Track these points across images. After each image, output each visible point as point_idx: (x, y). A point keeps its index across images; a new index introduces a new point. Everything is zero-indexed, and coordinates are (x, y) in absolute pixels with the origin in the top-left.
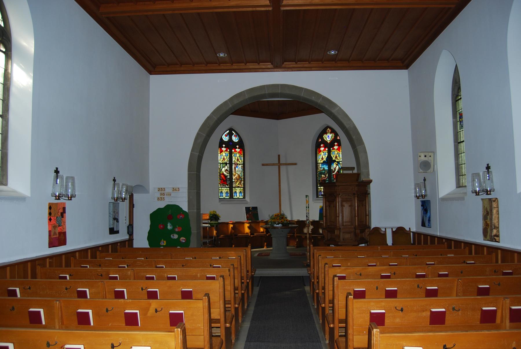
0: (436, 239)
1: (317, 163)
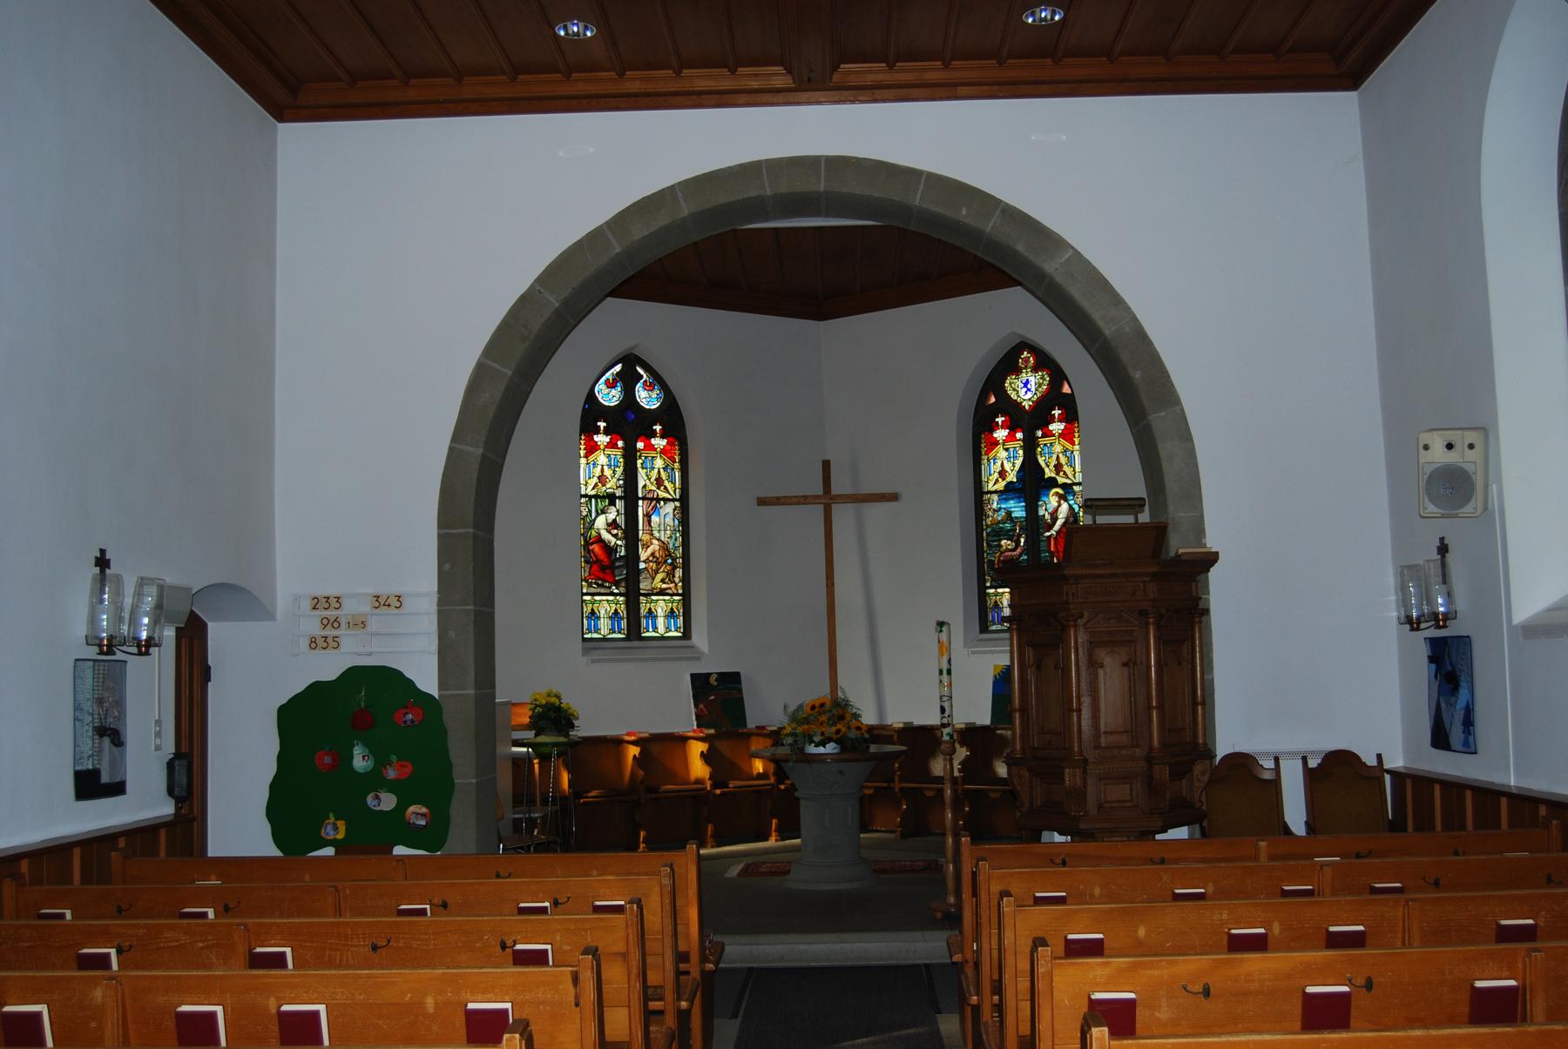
1: (979, 492)
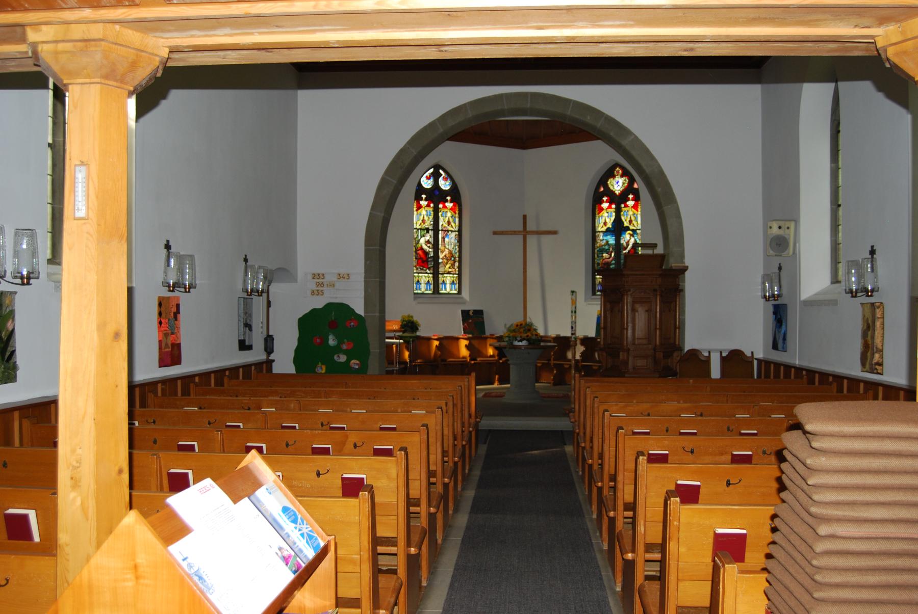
0: (793, 370)
